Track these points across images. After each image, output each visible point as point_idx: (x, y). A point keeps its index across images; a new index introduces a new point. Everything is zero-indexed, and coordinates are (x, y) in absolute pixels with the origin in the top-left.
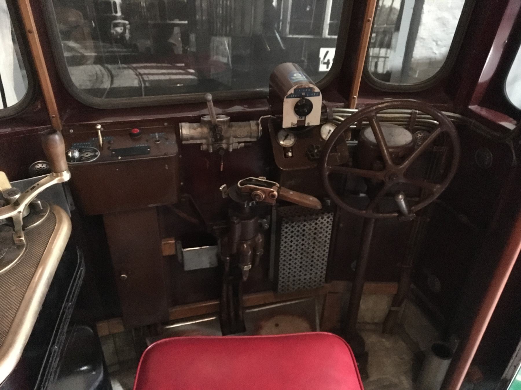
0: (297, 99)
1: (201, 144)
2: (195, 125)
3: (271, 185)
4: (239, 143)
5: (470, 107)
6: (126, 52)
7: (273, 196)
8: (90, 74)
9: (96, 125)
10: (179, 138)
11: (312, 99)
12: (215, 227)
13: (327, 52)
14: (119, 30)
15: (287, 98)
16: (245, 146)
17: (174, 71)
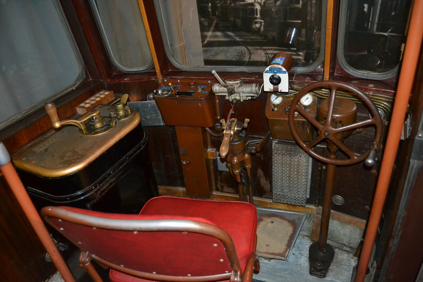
1: (225, 96)
4: (247, 96)
8: (238, 51)
14: (258, 25)
16: (252, 99)
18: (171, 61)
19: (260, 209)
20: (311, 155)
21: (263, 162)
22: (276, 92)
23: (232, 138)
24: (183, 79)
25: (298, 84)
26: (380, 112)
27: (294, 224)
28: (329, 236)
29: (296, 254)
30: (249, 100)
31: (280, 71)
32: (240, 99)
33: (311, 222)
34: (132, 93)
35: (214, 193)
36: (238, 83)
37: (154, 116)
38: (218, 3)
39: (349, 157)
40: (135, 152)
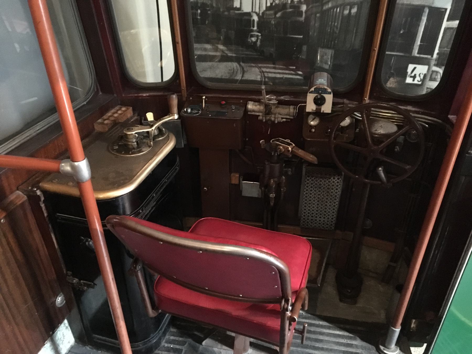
0: (315, 95)
1: (259, 116)
2: (257, 103)
3: (289, 144)
4: (282, 118)
5: (449, 116)
7: (289, 151)
9: (203, 96)
10: (246, 111)
11: (325, 96)
12: (258, 167)
13: (415, 68)
14: (254, 39)
17: (287, 72)
38: (209, 10)
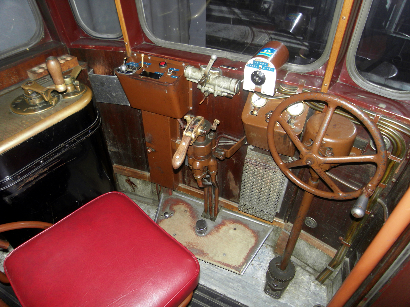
4: (222, 92)
6: (267, 22)
14: (266, 6)
15: (247, 65)
16: (227, 97)
17: (294, 41)
18: (145, 32)
19: (226, 211)
20: (286, 176)
21: (232, 167)
22: (258, 92)
23: (192, 142)
24: (154, 56)
25: (289, 86)
26: (385, 141)
27: (257, 235)
28: (294, 253)
29: (255, 265)
30: (224, 96)
31: (265, 66)
32: (214, 92)
33: (277, 235)
34: (98, 64)
35: (181, 185)
36: (215, 74)
37: (120, 94)
39: (332, 191)
40: (78, 139)
